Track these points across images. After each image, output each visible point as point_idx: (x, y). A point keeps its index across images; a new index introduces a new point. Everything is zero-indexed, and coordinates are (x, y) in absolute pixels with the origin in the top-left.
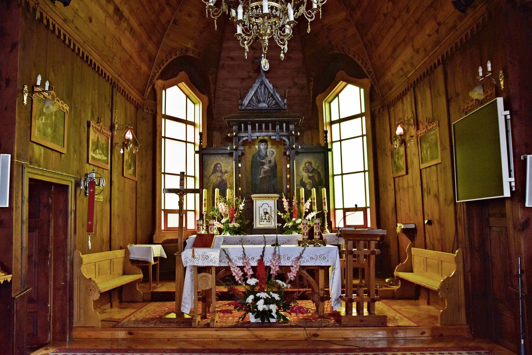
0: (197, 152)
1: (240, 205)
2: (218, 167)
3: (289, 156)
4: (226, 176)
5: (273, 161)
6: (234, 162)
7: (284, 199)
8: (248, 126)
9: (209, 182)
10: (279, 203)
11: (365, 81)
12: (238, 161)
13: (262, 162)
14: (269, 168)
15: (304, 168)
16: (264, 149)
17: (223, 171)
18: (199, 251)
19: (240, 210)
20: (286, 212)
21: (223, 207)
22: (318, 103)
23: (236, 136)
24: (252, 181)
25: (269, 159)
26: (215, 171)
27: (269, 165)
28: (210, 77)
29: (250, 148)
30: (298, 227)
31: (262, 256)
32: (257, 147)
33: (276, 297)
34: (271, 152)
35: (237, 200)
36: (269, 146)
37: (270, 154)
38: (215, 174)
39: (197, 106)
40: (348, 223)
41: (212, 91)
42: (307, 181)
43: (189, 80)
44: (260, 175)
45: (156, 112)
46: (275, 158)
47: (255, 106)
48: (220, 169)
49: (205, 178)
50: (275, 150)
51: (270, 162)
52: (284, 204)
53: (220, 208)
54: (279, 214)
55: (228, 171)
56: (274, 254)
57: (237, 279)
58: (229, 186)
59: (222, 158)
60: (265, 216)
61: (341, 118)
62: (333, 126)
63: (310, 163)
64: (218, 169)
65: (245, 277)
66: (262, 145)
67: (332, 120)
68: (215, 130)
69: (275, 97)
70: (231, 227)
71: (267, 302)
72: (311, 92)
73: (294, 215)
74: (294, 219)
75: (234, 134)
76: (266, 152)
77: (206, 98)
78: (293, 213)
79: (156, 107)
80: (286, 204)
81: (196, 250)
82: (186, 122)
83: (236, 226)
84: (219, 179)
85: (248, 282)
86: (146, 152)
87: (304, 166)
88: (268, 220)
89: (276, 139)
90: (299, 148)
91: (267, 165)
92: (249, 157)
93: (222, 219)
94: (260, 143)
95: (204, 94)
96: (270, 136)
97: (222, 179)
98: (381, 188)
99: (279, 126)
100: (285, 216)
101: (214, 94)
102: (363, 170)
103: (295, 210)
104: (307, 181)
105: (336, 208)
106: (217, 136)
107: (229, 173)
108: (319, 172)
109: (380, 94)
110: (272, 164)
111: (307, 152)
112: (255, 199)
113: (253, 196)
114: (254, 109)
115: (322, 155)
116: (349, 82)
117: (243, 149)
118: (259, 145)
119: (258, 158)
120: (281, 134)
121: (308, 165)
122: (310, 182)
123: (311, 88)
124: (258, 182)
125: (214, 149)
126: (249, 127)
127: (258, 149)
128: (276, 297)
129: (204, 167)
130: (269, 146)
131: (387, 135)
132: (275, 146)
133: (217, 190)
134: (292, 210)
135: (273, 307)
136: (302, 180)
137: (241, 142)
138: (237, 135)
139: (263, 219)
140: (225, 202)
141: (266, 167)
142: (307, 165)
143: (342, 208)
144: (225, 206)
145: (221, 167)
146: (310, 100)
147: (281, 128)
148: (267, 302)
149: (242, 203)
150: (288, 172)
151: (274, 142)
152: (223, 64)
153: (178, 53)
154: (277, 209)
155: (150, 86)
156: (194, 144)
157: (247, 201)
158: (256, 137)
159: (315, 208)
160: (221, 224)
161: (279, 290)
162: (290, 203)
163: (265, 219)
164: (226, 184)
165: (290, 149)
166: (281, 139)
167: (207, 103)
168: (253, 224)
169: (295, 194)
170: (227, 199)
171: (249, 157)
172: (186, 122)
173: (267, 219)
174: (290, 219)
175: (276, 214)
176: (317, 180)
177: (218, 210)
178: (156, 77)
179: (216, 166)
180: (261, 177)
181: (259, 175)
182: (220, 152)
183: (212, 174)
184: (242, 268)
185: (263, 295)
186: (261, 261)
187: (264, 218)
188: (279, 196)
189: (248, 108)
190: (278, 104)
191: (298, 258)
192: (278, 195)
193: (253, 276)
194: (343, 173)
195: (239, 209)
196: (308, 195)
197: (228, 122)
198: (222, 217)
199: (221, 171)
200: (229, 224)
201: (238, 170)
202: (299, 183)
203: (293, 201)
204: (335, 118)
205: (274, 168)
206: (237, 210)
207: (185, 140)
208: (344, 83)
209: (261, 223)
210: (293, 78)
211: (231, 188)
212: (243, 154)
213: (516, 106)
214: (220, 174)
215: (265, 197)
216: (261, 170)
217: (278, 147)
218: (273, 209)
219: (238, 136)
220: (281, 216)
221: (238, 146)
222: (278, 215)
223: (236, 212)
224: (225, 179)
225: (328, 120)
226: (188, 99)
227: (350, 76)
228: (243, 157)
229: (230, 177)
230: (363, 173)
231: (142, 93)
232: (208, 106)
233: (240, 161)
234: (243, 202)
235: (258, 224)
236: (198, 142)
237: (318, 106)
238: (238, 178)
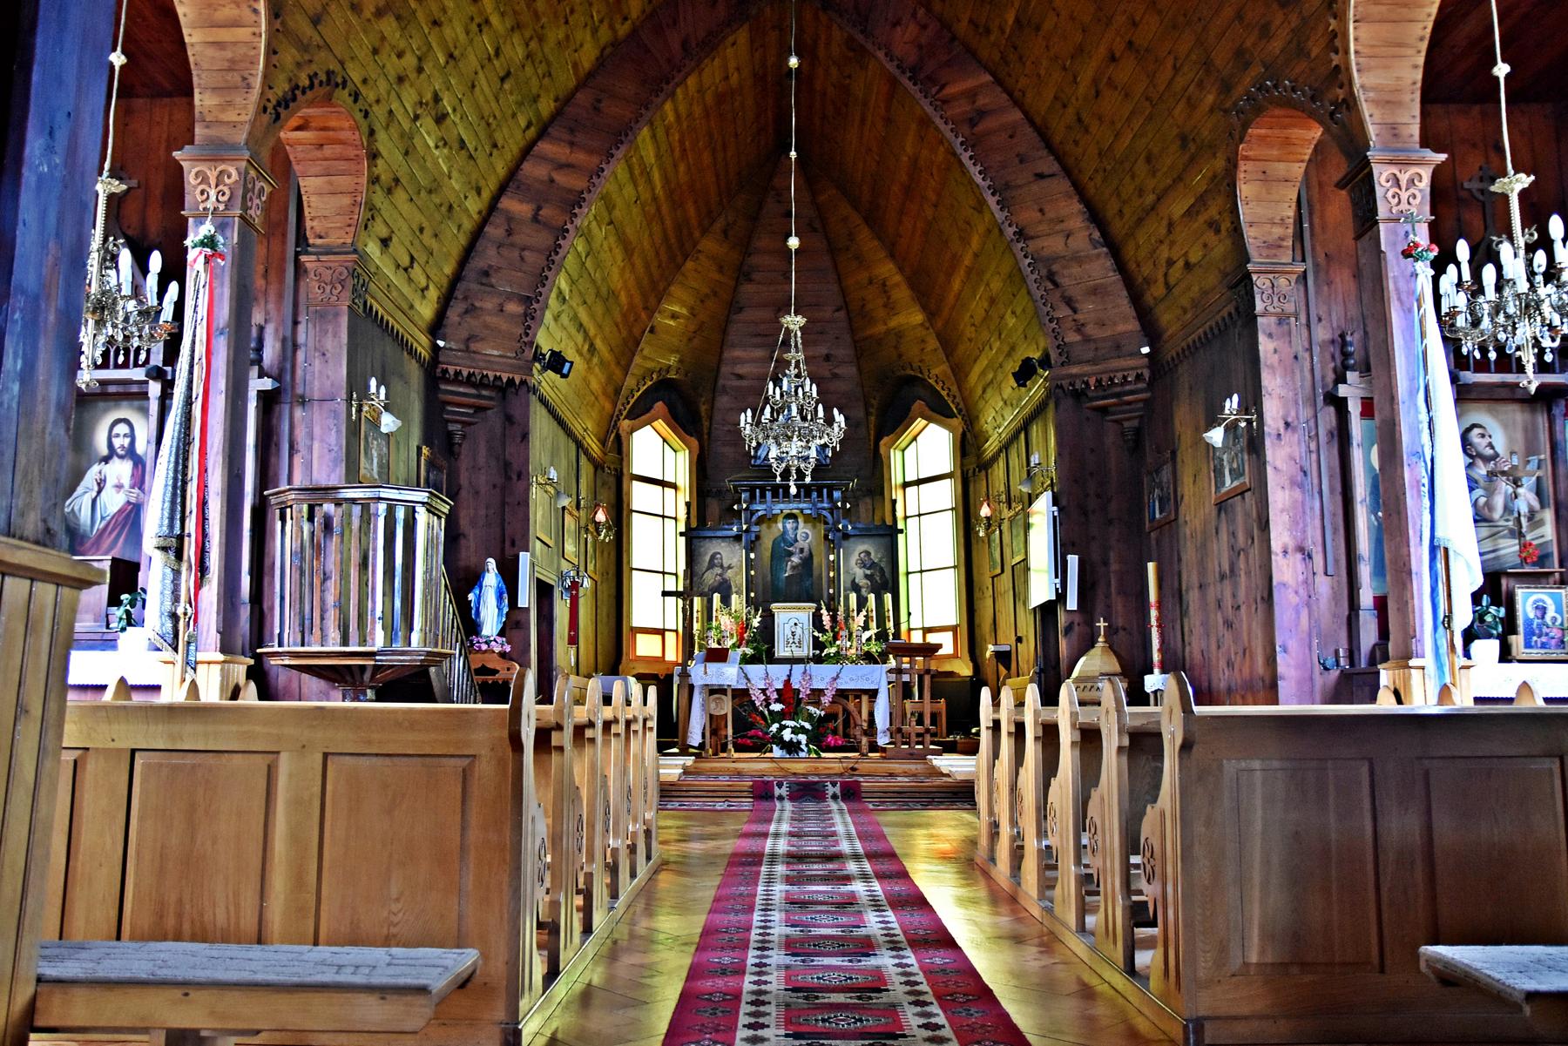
0: (681, 534)
3: (833, 541)
4: (729, 574)
5: (806, 550)
7: (824, 611)
12: (749, 549)
17: (725, 565)
18: (713, 667)
22: (882, 450)
23: (747, 509)
24: (772, 580)
26: (711, 565)
28: (703, 408)
29: (769, 527)
31: (789, 676)
32: (780, 525)
33: (808, 726)
35: (749, 612)
36: (801, 524)
39: (680, 454)
41: (706, 431)
42: (862, 582)
43: (669, 416)
51: (802, 550)
54: (816, 634)
56: (805, 673)
57: (758, 703)
58: (734, 589)
62: (908, 489)
63: (868, 553)
65: (767, 703)
71: (795, 731)
77: (695, 442)
79: (621, 464)
80: (826, 619)
81: (708, 664)
82: (662, 483)
85: (771, 708)
92: (767, 543)
96: (802, 510)
98: (977, 594)
101: (709, 434)
104: (862, 582)
106: (714, 507)
107: (735, 569)
108: (882, 569)
111: (865, 534)
113: (773, 606)
115: (887, 540)
116: (930, 420)
120: (820, 505)
124: (782, 585)
125: (710, 529)
126: (769, 494)
128: (808, 726)
130: (801, 524)
132: (810, 525)
133: (717, 597)
135: (803, 738)
136: (853, 581)
137: (754, 518)
141: (795, 559)
147: (820, 495)
148: (795, 731)
151: (808, 518)
153: (655, 376)
156: (675, 519)
159: (873, 625)
161: (810, 718)
162: (834, 619)
164: (730, 587)
166: (819, 515)
167: (696, 451)
171: (767, 543)
172: (662, 483)
179: (713, 557)
182: (720, 534)
184: (764, 691)
185: (791, 723)
186: (787, 683)
191: (835, 679)
193: (777, 701)
196: (862, 602)
197: (735, 487)
199: (722, 566)
201: (750, 564)
202: (849, 585)
205: (808, 561)
208: (924, 422)
211: (739, 593)
212: (758, 537)
213: (1064, 502)
214: (719, 571)
217: (814, 527)
218: (806, 627)
225: (900, 481)
227: (933, 410)
231: (603, 442)
232: (699, 457)
235: (781, 651)
236: (682, 516)
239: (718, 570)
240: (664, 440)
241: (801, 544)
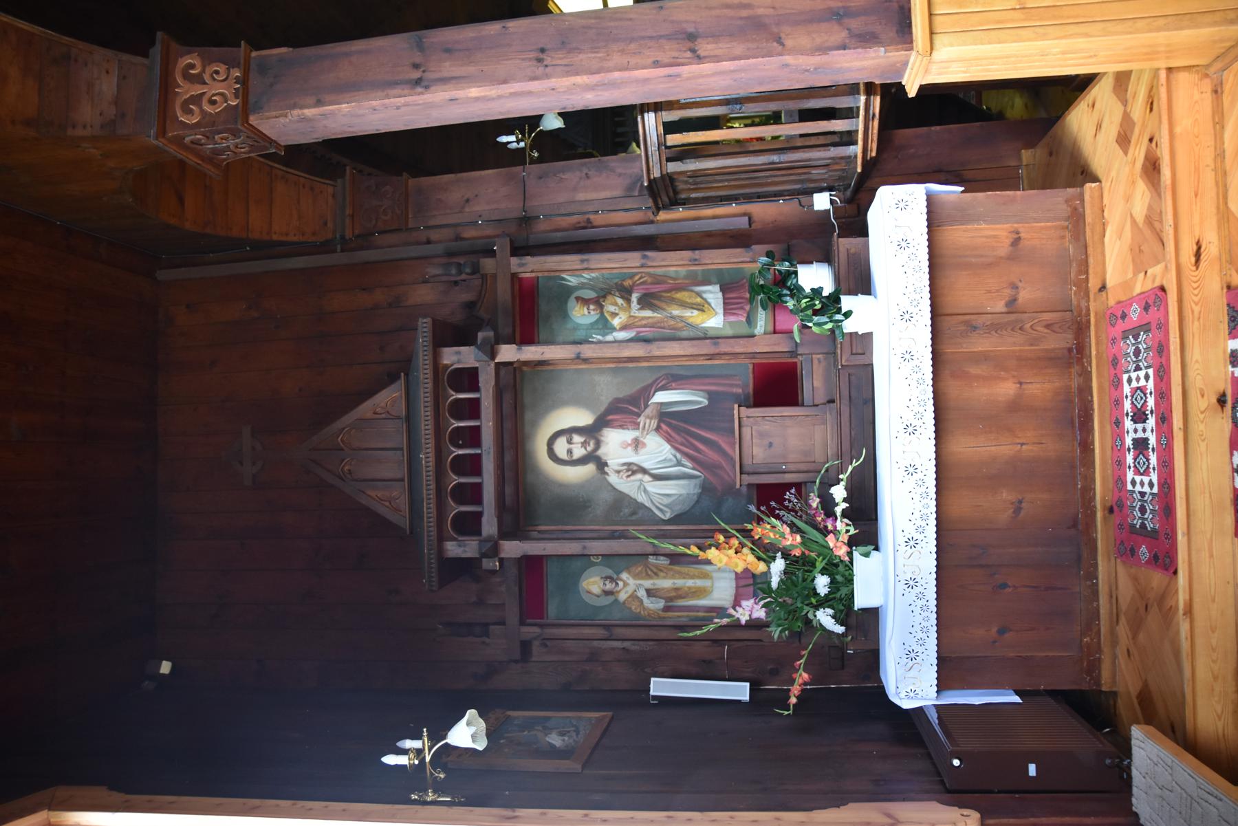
126: (620, 130)
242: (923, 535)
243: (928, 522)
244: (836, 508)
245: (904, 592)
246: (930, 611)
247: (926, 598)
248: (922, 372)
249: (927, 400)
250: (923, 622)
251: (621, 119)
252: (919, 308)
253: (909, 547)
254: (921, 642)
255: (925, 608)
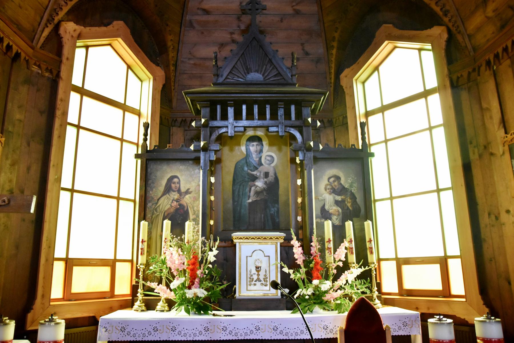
1: (210, 253)
2: (174, 183)
5: (271, 174)
6: (201, 171)
7: (295, 243)
8: (229, 108)
9: (156, 210)
10: (282, 248)
11: (437, 31)
13: (253, 175)
14: (265, 186)
15: (327, 185)
16: (256, 151)
17: (183, 190)
19: (210, 263)
20: (299, 266)
21: (176, 256)
22: (344, 82)
23: (206, 125)
25: (266, 171)
26: (168, 189)
27: (265, 180)
29: (231, 150)
30: (323, 298)
32: (243, 148)
34: (269, 158)
36: (266, 147)
37: (268, 162)
38: (167, 195)
40: (407, 286)
42: (333, 209)
44: (249, 197)
45: (58, 75)
46: (274, 168)
47: (242, 78)
48: (178, 185)
49: (150, 202)
50: (276, 154)
51: (266, 175)
52: (346, 272)
53: (168, 258)
54: (286, 270)
55: (190, 190)
59: (181, 167)
60: (258, 275)
61: (384, 104)
63: (338, 178)
64: (173, 185)
66: (253, 145)
67: (369, 109)
68: (174, 126)
69: (275, 64)
70: (191, 296)
72: (333, 65)
73: (315, 275)
74: (315, 282)
75: (203, 120)
76: (260, 158)
77: (161, 72)
78: (312, 268)
80: (298, 251)
82: (124, 107)
83: (200, 295)
84: (175, 203)
86: (29, 145)
87: (327, 182)
88: (263, 282)
89: (278, 132)
90: (319, 147)
91: (262, 180)
93: (174, 279)
94: (248, 143)
95: (158, 65)
97: (180, 205)
99: (283, 110)
100: (298, 275)
101: (176, 65)
102: (435, 188)
103: (317, 263)
104: (333, 209)
105: (381, 257)
109: (469, 47)
110: (271, 178)
112: (239, 241)
113: (235, 235)
114: (238, 82)
117: (218, 149)
118: (247, 146)
119: (246, 169)
121: (334, 181)
122: (338, 211)
123: (333, 59)
124: (245, 211)
126: (231, 111)
127: (245, 153)
129: (150, 182)
130: (266, 147)
131: (491, 117)
132: (275, 148)
134: (311, 262)
137: (214, 137)
138: (208, 124)
139: (255, 279)
140: (180, 247)
141: (260, 184)
142: (332, 180)
143: (394, 257)
144: (179, 255)
145: (179, 183)
146: (331, 78)
149: (214, 249)
150: (299, 194)
152: (190, 21)
154: (281, 260)
155: (47, 27)
156: (137, 145)
157: (223, 244)
158: (242, 129)
160: (171, 290)
163: (258, 280)
165: (303, 150)
168: (235, 289)
169: (315, 233)
170: (186, 241)
172: (124, 107)
173: (262, 279)
174: (306, 280)
175: (279, 270)
176: (351, 208)
177: (164, 262)
178: (61, 14)
180: (250, 201)
181: (247, 198)
183: (164, 194)
187: (255, 277)
188: (285, 235)
189: (229, 80)
190: (281, 75)
192: (283, 235)
194: (440, 187)
195: (207, 259)
198: (174, 277)
199: (179, 191)
200: (187, 291)
201: (209, 189)
203: (312, 246)
204: (373, 104)
206: (204, 261)
207: (120, 137)
209: (249, 288)
210: (302, 44)
214: (175, 195)
215: (259, 238)
216: (250, 189)
217: (280, 150)
219: (210, 125)
220: (289, 274)
221: (209, 143)
222: (283, 273)
223: (202, 266)
224: (185, 205)
225: (363, 111)
226: (129, 70)
228: (218, 166)
229: (194, 201)
230: (390, 201)
233: (212, 174)
234: (216, 247)
237: (344, 88)
238: (208, 204)
239: (175, 195)
240: (129, 67)
241: (266, 167)
242: (228, 334)
243: (285, 335)
244: (377, 289)
245: (253, 325)
246: (295, 336)
247: (149, 336)
248: (199, 336)
249: (288, 336)
250: (138, 334)
251: (268, 116)
252: (177, 335)
253: (274, 327)
254: (180, 333)
255: (144, 335)
